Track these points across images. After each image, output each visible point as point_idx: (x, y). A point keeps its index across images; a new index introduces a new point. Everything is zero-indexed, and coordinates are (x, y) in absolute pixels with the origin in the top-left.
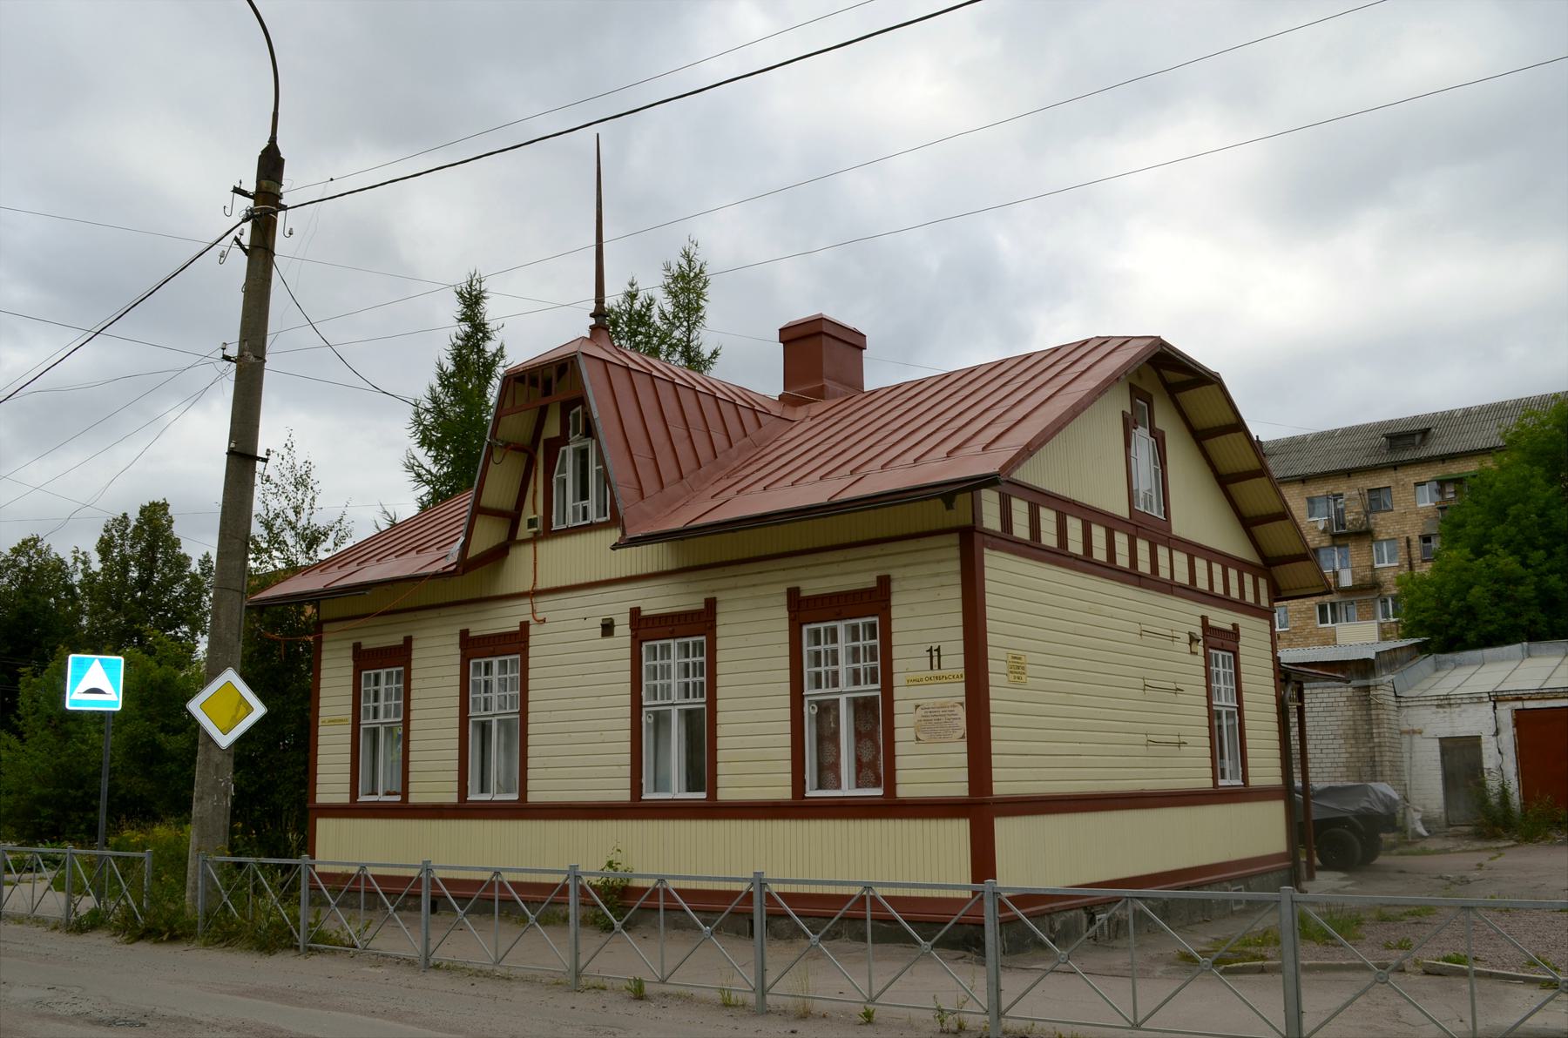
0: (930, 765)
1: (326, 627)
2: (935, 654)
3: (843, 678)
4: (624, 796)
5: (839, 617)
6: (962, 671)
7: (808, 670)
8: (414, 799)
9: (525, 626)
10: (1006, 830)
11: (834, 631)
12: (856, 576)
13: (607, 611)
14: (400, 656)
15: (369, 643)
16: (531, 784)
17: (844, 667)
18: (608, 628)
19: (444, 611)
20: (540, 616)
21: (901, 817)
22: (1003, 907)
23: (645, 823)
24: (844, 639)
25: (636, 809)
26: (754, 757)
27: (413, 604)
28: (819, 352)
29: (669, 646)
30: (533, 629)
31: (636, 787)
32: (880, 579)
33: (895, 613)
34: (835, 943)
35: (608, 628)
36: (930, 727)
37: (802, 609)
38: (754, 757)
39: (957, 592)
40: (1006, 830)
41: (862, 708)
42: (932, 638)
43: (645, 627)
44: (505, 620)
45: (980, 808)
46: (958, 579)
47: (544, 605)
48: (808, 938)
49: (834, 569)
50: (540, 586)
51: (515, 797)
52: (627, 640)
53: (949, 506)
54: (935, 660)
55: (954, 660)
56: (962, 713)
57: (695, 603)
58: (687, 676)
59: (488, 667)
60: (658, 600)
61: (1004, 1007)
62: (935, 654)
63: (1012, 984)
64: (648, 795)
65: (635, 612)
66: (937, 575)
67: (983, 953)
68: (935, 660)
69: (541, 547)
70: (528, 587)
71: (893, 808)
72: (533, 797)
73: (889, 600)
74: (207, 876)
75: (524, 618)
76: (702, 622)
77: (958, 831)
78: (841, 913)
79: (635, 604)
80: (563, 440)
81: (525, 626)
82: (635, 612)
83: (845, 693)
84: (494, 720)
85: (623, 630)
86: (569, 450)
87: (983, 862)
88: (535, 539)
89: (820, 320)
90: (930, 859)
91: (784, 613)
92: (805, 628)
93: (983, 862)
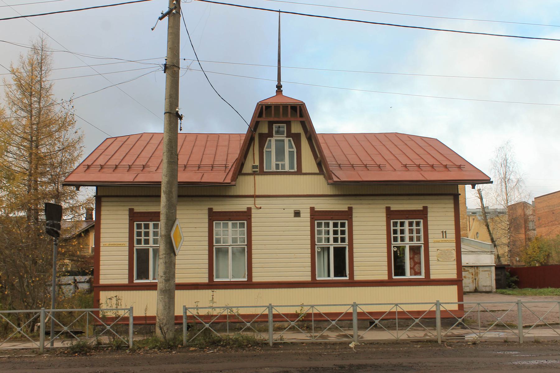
0: (442, 268)
1: (103, 199)
2: (444, 233)
3: (151, 241)
4: (309, 279)
6: (454, 239)
9: (249, 209)
13: (297, 207)
14: (423, 214)
16: (355, 273)
17: (407, 235)
20: (258, 206)
21: (304, 287)
25: (314, 283)
32: (424, 207)
33: (429, 219)
35: (297, 214)
39: (453, 214)
41: (415, 250)
42: (444, 228)
43: (316, 216)
44: (240, 206)
46: (453, 210)
47: (259, 201)
48: (76, 339)
50: (257, 194)
54: (444, 235)
55: (451, 235)
60: (322, 205)
62: (444, 233)
65: (312, 209)
66: (445, 208)
67: (435, 326)
68: (444, 235)
69: (257, 177)
70: (252, 193)
71: (428, 282)
72: (255, 280)
73: (427, 214)
76: (348, 215)
78: (381, 318)
79: (312, 206)
80: (270, 135)
81: (249, 209)
82: (312, 209)
83: (407, 244)
84: (230, 248)
85: (306, 216)
86: (273, 140)
88: (254, 174)
91: (385, 215)
92: (135, 223)
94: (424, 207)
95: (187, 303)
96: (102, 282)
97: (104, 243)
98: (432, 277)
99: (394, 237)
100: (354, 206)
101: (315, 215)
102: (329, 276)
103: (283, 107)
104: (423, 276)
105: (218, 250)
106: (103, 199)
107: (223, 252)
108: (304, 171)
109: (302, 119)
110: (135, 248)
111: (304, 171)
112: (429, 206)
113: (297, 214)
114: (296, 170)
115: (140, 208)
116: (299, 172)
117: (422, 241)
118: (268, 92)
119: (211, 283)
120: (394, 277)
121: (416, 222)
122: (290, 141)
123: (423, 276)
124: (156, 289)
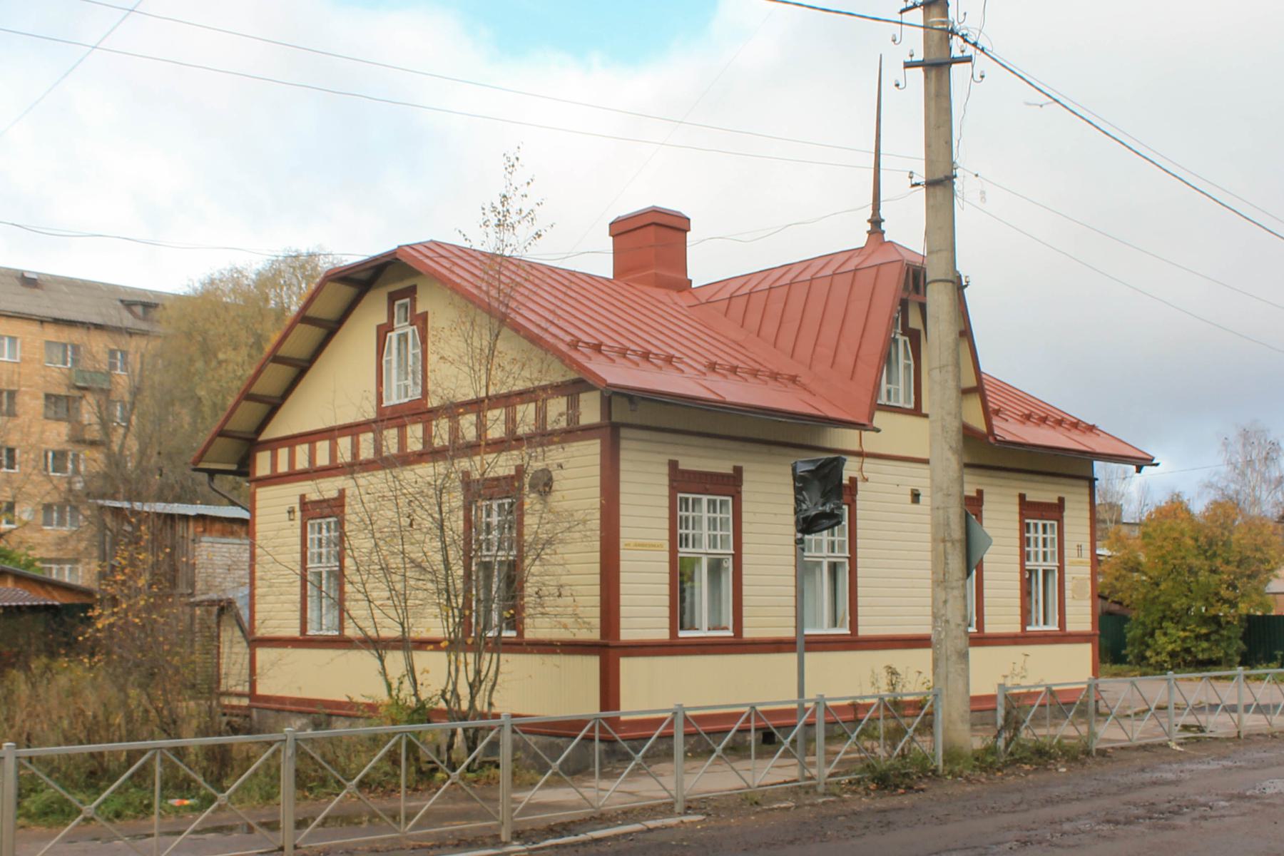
2: (1079, 547)
5: (1041, 518)
8: (863, 631)
10: (629, 667)
11: (1036, 525)
15: (1032, 496)
18: (916, 497)
19: (775, 449)
27: (793, 441)
28: (652, 240)
29: (700, 500)
30: (860, 485)
31: (799, 624)
35: (916, 497)
40: (629, 667)
45: (609, 649)
51: (1056, 628)
57: (722, 466)
58: (715, 529)
62: (1079, 547)
64: (311, 632)
71: (738, 645)
77: (591, 665)
87: (609, 694)
89: (655, 211)
90: (566, 690)
93: (609, 694)
97: (627, 541)
112: (745, 466)
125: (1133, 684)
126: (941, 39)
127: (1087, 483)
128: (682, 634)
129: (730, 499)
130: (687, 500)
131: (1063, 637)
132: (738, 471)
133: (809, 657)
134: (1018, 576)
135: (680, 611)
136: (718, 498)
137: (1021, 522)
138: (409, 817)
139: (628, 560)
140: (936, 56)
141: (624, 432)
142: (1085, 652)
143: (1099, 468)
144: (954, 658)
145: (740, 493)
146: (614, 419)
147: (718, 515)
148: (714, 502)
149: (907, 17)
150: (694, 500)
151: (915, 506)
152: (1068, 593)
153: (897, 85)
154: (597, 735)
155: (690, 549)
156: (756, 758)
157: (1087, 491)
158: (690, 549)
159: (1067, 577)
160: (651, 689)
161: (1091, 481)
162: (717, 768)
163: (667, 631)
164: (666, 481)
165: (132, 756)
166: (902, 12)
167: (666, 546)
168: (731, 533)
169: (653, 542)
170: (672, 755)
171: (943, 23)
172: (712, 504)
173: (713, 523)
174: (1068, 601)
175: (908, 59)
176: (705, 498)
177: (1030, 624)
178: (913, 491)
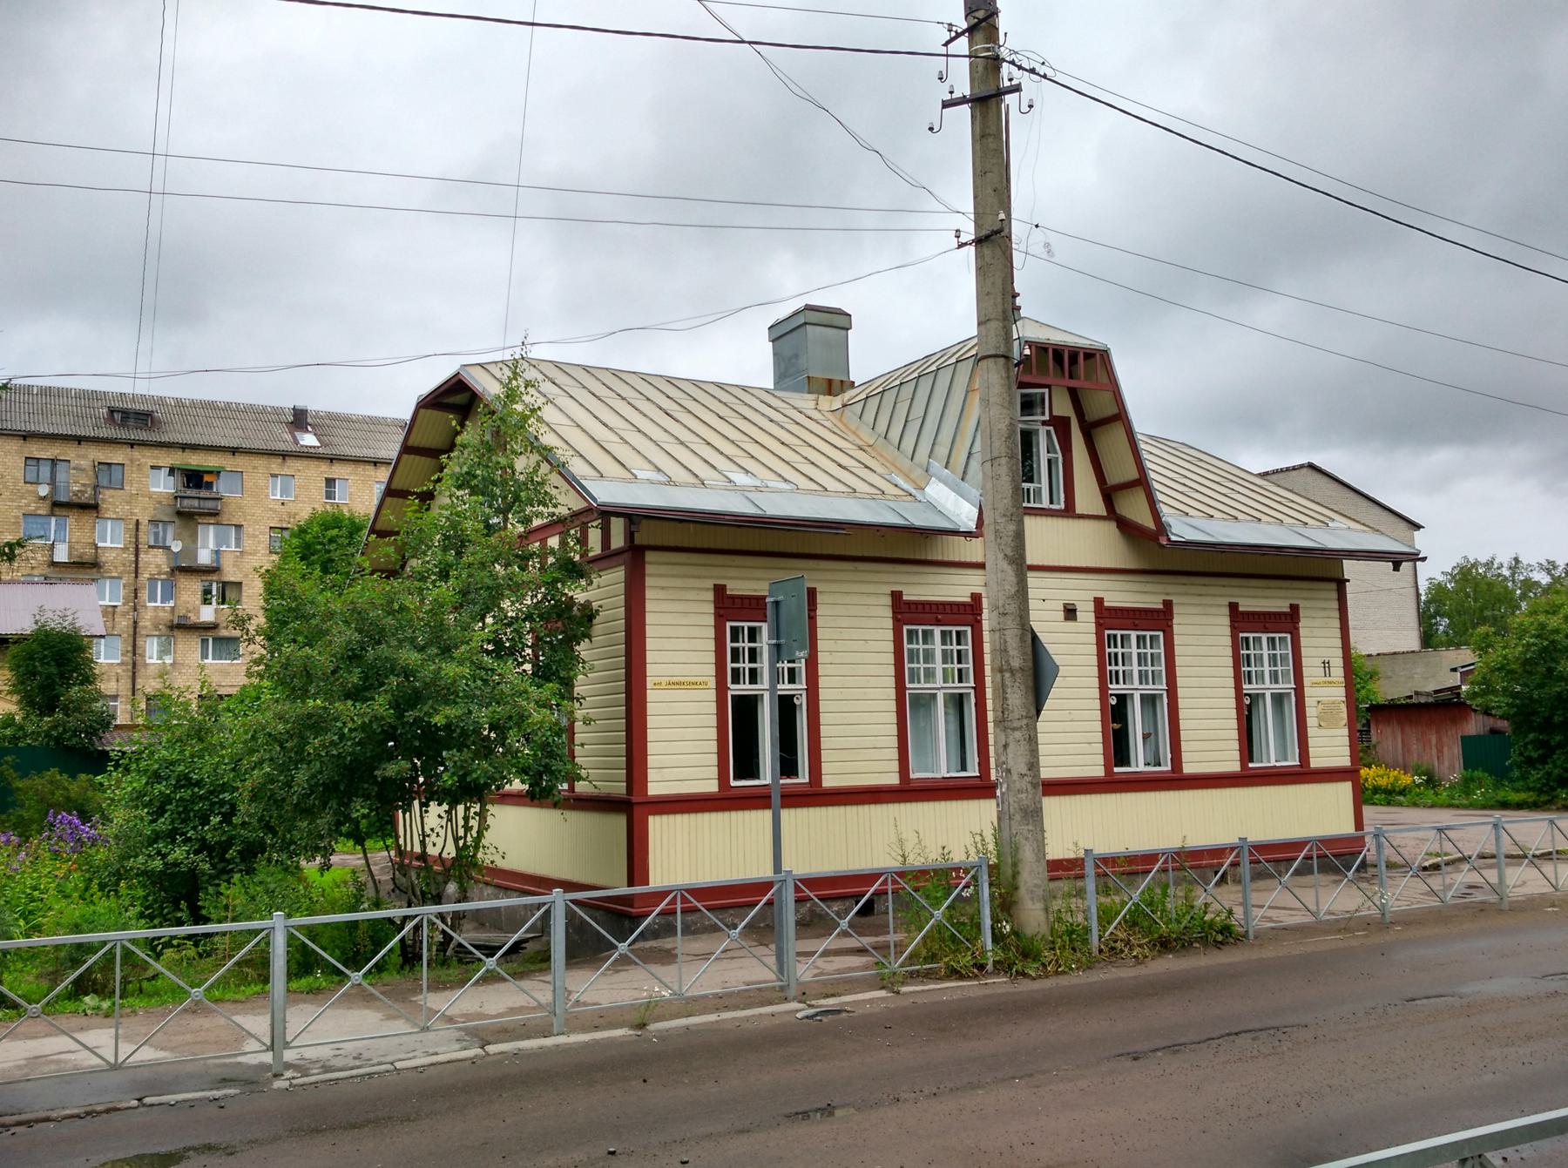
2: (1326, 665)
4: (893, 779)
5: (1266, 631)
7: (969, 665)
10: (659, 827)
12: (1274, 602)
13: (1071, 597)
14: (1288, 621)
15: (1246, 605)
16: (1185, 757)
17: (938, 665)
22: (1097, 866)
23: (812, 810)
24: (1262, 646)
26: (1209, 739)
32: (1292, 606)
33: (1302, 632)
34: (1308, 879)
36: (1326, 720)
37: (1241, 621)
38: (1209, 739)
40: (659, 827)
49: (1259, 592)
52: (1092, 627)
53: (1396, 567)
56: (1344, 708)
57: (1153, 601)
59: (927, 636)
60: (1120, 595)
61: (289, 1039)
63: (298, 1018)
65: (1098, 602)
71: (1177, 780)
72: (1315, 763)
74: (105, 943)
75: (977, 590)
76: (1160, 619)
78: (658, 909)
79: (1099, 595)
82: (1098, 602)
85: (1087, 616)
93: (636, 866)
94: (1292, 606)
95: (1081, 828)
96: (654, 789)
97: (657, 680)
98: (828, 782)
99: (733, 669)
100: (1175, 600)
101: (1106, 617)
102: (964, 768)
103: (1055, 351)
104: (1166, 767)
105: (917, 699)
106: (650, 556)
107: (924, 702)
108: (1079, 511)
109: (1073, 383)
110: (730, 693)
111: (1079, 511)
112: (1302, 604)
113: (1070, 613)
114: (1062, 506)
115: (741, 586)
116: (1069, 511)
117: (801, 685)
118: (1023, 313)
119: (906, 787)
120: (733, 783)
121: (750, 629)
122: (1048, 433)
123: (1166, 767)
124: (993, 796)
125: (1552, 822)
126: (986, 68)
127: (1334, 586)
128: (1116, 770)
129: (1161, 634)
130: (1247, 639)
131: (1304, 774)
132: (1295, 609)
133: (787, 815)
134: (1233, 703)
135: (1118, 748)
136: (1277, 636)
137: (1234, 637)
138: (899, 953)
139: (656, 702)
140: (983, 91)
141: (650, 556)
142: (1343, 792)
143: (1350, 568)
144: (1018, 817)
145: (1171, 627)
146: (638, 540)
147: (1278, 652)
148: (1273, 639)
149: (952, 48)
150: (750, 629)
151: (1070, 624)
152: (1311, 722)
153: (931, 129)
154: (679, 906)
155: (1121, 686)
156: (429, 989)
157: (1334, 595)
158: (1121, 686)
159: (1309, 702)
160: (686, 853)
161: (1341, 583)
162: (617, 977)
163: (897, 776)
164: (710, 608)
165: (405, 919)
166: (946, 45)
167: (712, 683)
168: (971, 665)
169: (694, 679)
170: (548, 959)
171: (988, 50)
172: (1272, 641)
173: (1142, 659)
174: (1311, 732)
175: (948, 97)
176: (1133, 634)
177: (1251, 760)
178: (1065, 605)
